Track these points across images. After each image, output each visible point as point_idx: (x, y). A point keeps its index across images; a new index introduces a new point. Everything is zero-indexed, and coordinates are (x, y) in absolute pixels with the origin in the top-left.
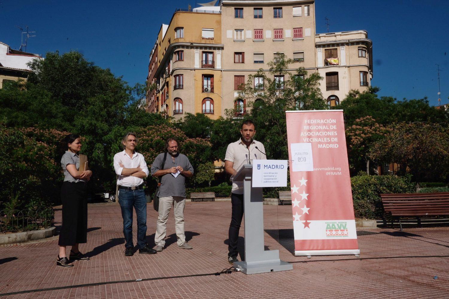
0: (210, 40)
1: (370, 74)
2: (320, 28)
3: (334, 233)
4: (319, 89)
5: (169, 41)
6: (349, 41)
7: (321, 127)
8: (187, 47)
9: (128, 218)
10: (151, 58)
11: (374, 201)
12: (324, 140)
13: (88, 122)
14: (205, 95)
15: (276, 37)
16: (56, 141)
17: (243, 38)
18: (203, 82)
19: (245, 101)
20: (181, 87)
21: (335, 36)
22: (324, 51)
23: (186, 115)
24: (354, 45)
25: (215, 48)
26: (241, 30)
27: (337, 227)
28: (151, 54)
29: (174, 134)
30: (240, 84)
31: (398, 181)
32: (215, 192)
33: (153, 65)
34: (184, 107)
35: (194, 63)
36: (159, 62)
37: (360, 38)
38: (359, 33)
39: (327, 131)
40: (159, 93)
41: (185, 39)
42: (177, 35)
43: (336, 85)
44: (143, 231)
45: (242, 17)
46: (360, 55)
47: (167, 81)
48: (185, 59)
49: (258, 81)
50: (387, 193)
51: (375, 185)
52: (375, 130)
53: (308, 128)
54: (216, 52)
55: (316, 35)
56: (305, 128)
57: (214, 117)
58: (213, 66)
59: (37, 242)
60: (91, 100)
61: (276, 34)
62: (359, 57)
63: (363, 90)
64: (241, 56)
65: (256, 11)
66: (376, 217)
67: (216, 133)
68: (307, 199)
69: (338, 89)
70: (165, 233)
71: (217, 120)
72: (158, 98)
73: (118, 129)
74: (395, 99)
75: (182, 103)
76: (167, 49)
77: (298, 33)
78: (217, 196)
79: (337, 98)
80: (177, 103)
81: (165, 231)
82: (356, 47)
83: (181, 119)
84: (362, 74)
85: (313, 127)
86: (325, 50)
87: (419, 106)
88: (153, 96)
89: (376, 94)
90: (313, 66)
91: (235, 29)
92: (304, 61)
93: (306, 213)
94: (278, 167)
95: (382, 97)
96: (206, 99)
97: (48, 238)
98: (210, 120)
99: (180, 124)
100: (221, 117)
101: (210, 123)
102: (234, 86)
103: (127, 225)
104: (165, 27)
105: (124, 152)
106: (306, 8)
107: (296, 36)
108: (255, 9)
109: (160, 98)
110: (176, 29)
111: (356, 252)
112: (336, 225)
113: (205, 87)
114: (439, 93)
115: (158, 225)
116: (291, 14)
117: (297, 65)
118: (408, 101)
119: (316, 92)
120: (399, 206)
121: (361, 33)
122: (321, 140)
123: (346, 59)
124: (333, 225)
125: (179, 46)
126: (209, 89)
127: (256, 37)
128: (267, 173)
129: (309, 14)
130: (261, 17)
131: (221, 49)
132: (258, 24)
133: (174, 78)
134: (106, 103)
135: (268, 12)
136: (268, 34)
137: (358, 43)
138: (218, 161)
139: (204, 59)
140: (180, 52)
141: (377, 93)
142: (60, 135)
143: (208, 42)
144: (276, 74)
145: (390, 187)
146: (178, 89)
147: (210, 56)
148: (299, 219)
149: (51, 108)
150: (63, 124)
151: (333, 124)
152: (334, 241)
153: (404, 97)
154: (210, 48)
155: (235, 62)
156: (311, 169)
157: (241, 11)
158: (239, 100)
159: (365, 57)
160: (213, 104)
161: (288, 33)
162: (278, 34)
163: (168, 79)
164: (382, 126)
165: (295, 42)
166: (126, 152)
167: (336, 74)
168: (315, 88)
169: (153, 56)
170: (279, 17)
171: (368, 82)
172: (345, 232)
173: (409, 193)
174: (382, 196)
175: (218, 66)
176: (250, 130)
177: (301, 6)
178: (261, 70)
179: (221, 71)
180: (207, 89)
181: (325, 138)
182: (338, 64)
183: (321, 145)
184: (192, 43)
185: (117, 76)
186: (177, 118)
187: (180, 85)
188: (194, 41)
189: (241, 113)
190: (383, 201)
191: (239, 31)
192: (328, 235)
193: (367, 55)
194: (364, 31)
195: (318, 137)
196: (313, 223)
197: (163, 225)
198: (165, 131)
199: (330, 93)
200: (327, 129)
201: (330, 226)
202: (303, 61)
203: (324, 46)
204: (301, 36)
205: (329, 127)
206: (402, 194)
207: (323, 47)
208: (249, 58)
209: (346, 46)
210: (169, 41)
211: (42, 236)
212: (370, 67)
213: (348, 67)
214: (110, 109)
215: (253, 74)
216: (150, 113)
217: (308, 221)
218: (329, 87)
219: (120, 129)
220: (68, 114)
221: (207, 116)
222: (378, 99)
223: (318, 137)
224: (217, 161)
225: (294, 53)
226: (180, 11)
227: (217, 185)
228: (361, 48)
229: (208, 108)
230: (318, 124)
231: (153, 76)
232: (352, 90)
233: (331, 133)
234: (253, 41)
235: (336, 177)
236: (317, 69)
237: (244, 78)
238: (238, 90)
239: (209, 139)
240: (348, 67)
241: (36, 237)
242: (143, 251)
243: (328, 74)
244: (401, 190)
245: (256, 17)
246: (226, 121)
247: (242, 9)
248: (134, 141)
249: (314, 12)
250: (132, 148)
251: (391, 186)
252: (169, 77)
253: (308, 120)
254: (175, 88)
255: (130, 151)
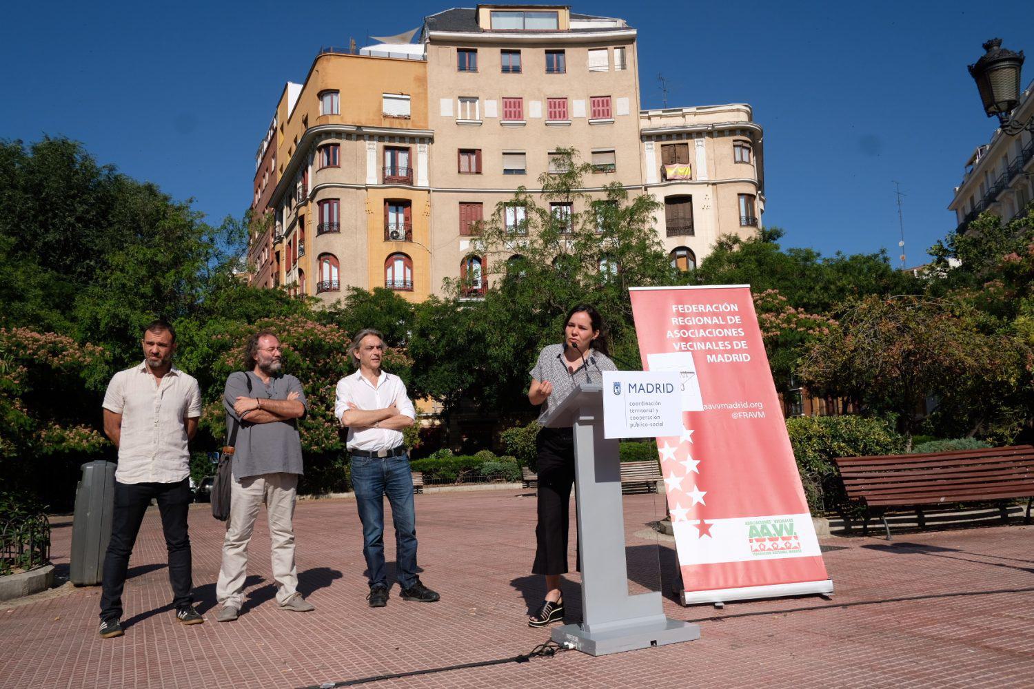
0: (403, 122)
1: (761, 199)
2: (648, 101)
3: (768, 544)
4: (654, 231)
5: (305, 122)
6: (713, 126)
7: (706, 320)
8: (349, 136)
9: (372, 521)
10: (260, 160)
11: (820, 474)
12: (717, 345)
13: (108, 310)
14: (392, 247)
15: (597, 114)
16: (26, 357)
17: (478, 118)
18: (386, 217)
19: (485, 260)
20: (335, 228)
21: (683, 116)
22: (660, 148)
23: (351, 293)
24: (724, 136)
25: (413, 139)
26: (473, 99)
27: (773, 531)
28: (260, 151)
29: (322, 336)
30: (471, 222)
31: (871, 429)
32: (424, 473)
33: (264, 176)
34: (341, 274)
35: (365, 174)
36: (281, 170)
37: (736, 120)
38: (733, 110)
39: (722, 327)
40: (281, 242)
41: (342, 118)
42: (323, 107)
43: (688, 224)
44: (407, 551)
45: (474, 69)
46: (738, 159)
47: (300, 214)
48: (343, 164)
49: (512, 217)
50: (848, 456)
51: (821, 437)
52: (788, 321)
53: (680, 321)
54: (417, 148)
55: (641, 113)
56: (673, 322)
57: (416, 298)
58: (409, 180)
59: (8, 607)
60: (116, 259)
61: (553, 110)
62: (736, 162)
63: (747, 234)
64: (473, 158)
65: (507, 57)
66: (826, 513)
67: (423, 333)
68: (697, 471)
69: (692, 233)
70: (245, 573)
71: (423, 305)
72: (278, 254)
73: (186, 328)
74: (819, 255)
75: (338, 266)
76: (299, 141)
77: (601, 108)
78: (429, 481)
79: (691, 254)
80: (326, 266)
81: (245, 568)
82: (728, 141)
83: (339, 302)
84: (742, 201)
85: (691, 319)
86: (662, 146)
87: (869, 269)
88: (266, 250)
89: (776, 242)
90: (637, 182)
91: (459, 97)
92: (615, 169)
93: (699, 503)
94: (661, 389)
95: (791, 250)
96: (394, 257)
97: (35, 596)
98: (406, 304)
99: (336, 314)
100: (432, 296)
101: (406, 311)
102: (458, 226)
103: (371, 537)
104: (294, 90)
105: (358, 372)
106: (617, 52)
107: (508, 115)
108: (503, 52)
109: (283, 255)
110: (322, 95)
111: (825, 586)
112: (770, 527)
113: (392, 228)
114: (901, 244)
115: (226, 555)
116: (585, 66)
117: (605, 180)
118: (847, 259)
119: (648, 238)
120: (897, 482)
121: (738, 110)
122: (712, 346)
123: (708, 166)
124: (764, 527)
125: (328, 134)
126: (402, 232)
127: (507, 115)
128: (637, 404)
129: (623, 66)
130: (517, 70)
131: (427, 140)
132: (512, 85)
133: (317, 207)
134: (154, 268)
135: (533, 59)
136: (535, 110)
137: (732, 131)
138: (426, 400)
139: (388, 164)
140: (331, 147)
141: (779, 241)
142: (37, 341)
143: (396, 124)
144: (557, 199)
145: (854, 441)
146: (327, 232)
147: (402, 158)
148: (685, 518)
149: (9, 275)
150: (42, 313)
151: (733, 314)
152: (771, 562)
153: (837, 251)
154: (402, 138)
155: (459, 172)
156: (698, 406)
157: (472, 56)
158: (473, 258)
159: (749, 163)
160: (411, 268)
161: (579, 108)
162: (557, 110)
163: (302, 211)
164: (802, 312)
165: (595, 127)
166: (363, 372)
167: (687, 199)
168: (646, 230)
169: (264, 156)
170: (558, 71)
171: (757, 217)
172: (793, 542)
173: (895, 454)
174: (839, 464)
175: (421, 180)
176: (160, 344)
177: (606, 49)
178: (521, 190)
179: (429, 191)
180: (397, 232)
181: (720, 343)
182: (691, 178)
183: (714, 356)
184: (359, 127)
185: (177, 199)
186: (328, 300)
187: (331, 224)
188: (363, 121)
189: (475, 288)
190: (843, 475)
191: (468, 102)
192: (756, 550)
193: (753, 160)
194: (746, 106)
195: (705, 340)
196: (717, 525)
197: (238, 554)
198: (300, 330)
199: (675, 242)
200: (721, 323)
201: (757, 530)
202: (614, 171)
203: (658, 137)
204: (608, 114)
205: (725, 319)
206: (881, 457)
207: (656, 141)
208: (492, 163)
209: (707, 138)
210: (305, 122)
211: (19, 589)
212: (760, 185)
213: (714, 184)
214: (163, 282)
215: (510, 198)
216: (259, 287)
217: (707, 522)
218: (673, 230)
219: (189, 326)
220: (57, 291)
221: (398, 296)
222: (781, 254)
223: (705, 340)
224: (422, 400)
225: (593, 153)
226: (329, 52)
227: (427, 456)
228: (739, 143)
229: (399, 276)
230: (702, 314)
231: (264, 203)
232: (725, 235)
233: (732, 332)
234: (501, 124)
235: (755, 422)
236: (646, 189)
237: (482, 207)
238: (472, 235)
239: (405, 349)
240: (714, 184)
241: (6, 594)
242: (411, 596)
243: (670, 200)
244: (878, 448)
245: (505, 70)
246: (445, 306)
247: (475, 51)
248: (378, 347)
249: (636, 61)
250: (375, 364)
251: (856, 440)
252: (306, 204)
253: (680, 306)
254: (321, 231)
255: (370, 371)
